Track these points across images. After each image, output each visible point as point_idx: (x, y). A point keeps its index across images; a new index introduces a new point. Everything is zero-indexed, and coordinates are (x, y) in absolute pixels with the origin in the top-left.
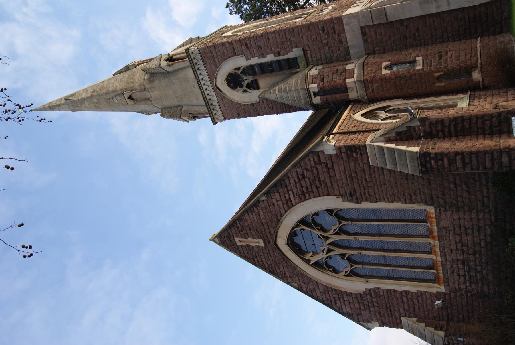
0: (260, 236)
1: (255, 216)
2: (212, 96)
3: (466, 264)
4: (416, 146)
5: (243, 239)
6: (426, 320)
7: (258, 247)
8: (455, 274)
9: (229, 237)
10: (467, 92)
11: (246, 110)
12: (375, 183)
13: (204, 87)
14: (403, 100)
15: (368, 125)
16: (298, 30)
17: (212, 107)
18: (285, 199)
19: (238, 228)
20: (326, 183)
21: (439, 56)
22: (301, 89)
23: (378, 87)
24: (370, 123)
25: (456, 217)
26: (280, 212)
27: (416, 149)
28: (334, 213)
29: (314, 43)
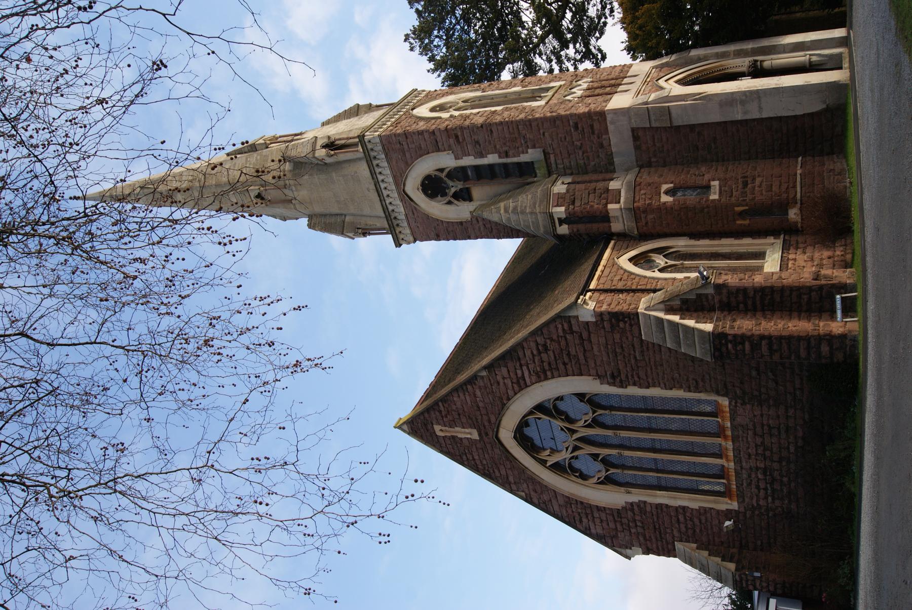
0: (474, 424)
1: (468, 398)
2: (396, 205)
3: (768, 473)
4: (708, 322)
5: (447, 428)
6: (710, 547)
7: (470, 440)
8: (753, 486)
9: (426, 425)
10: (780, 235)
11: (450, 229)
12: (648, 363)
13: (385, 193)
14: (690, 239)
15: (640, 279)
16: (538, 125)
17: (395, 222)
18: (515, 376)
19: (440, 412)
20: (578, 359)
21: (743, 182)
22: (540, 213)
23: (655, 219)
24: (642, 276)
25: (758, 412)
26: (507, 393)
27: (708, 327)
28: (587, 398)
29: (561, 144)
